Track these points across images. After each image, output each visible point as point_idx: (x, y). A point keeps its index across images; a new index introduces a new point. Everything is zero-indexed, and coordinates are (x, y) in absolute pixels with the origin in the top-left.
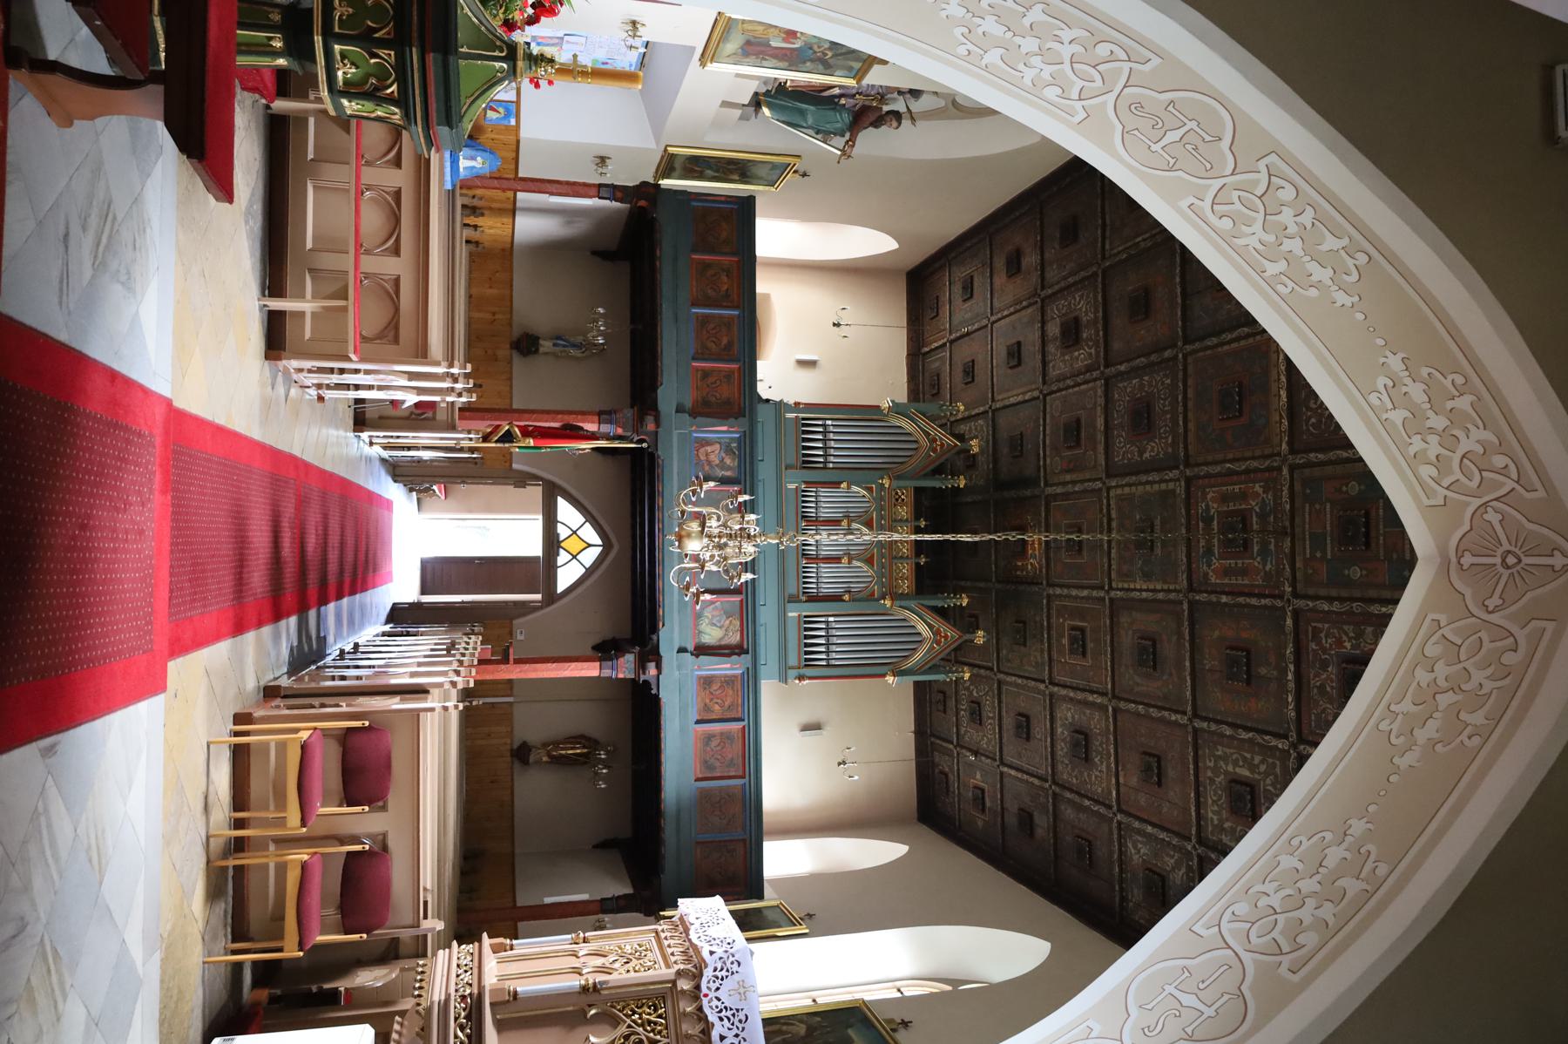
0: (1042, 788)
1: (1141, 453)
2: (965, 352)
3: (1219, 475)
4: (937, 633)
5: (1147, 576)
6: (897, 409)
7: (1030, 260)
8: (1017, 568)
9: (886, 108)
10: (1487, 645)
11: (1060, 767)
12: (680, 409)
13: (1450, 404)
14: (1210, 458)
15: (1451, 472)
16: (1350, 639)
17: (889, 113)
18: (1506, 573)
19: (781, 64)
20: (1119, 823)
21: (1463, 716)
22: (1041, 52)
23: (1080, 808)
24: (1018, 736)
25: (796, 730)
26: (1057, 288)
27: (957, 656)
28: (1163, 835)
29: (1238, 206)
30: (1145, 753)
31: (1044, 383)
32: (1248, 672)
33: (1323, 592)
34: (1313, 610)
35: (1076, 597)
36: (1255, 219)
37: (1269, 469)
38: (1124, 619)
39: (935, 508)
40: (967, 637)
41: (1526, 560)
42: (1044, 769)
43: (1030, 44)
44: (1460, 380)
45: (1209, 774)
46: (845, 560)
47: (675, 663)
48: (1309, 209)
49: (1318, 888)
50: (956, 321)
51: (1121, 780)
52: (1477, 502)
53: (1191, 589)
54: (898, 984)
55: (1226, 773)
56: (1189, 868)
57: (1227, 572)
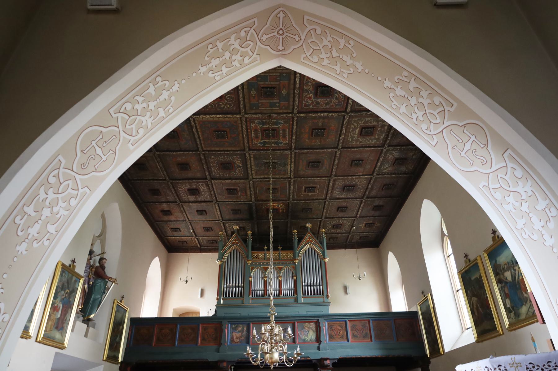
0: (365, 202)
1: (240, 167)
2: (200, 231)
3: (248, 139)
4: (308, 242)
5: (286, 165)
6: (221, 258)
7: (165, 207)
8: (283, 212)
9: (98, 264)
10: (314, 40)
11: (357, 196)
12: (218, 351)
13: (220, 50)
14: (242, 142)
15: (247, 52)
16: (308, 94)
17: (99, 263)
18: (286, 34)
19: (69, 312)
20: (377, 175)
21: (341, 47)
22: (51, 207)
23: (372, 188)
24: (345, 211)
25: (347, 296)
26: (176, 197)
27: (316, 234)
28: (381, 159)
29: (133, 126)
30: (351, 166)
31: (212, 202)
32: (321, 129)
33: (291, 103)
34: (298, 106)
35: (293, 190)
36: (140, 120)
37: (246, 121)
38: (301, 173)
39: (260, 243)
40: (309, 230)
41: (281, 27)
42: (358, 202)
43: (46, 212)
44: (211, 46)
45: (358, 143)
46: (280, 279)
47: (324, 351)
48: (135, 98)
49: (414, 98)
50: (188, 234)
51: (361, 174)
52: (259, 43)
53: (290, 149)
54: (446, 257)
55: (358, 137)
56: (393, 150)
57: (284, 136)
